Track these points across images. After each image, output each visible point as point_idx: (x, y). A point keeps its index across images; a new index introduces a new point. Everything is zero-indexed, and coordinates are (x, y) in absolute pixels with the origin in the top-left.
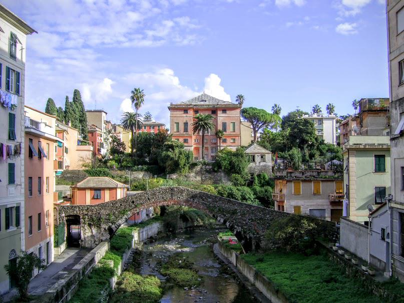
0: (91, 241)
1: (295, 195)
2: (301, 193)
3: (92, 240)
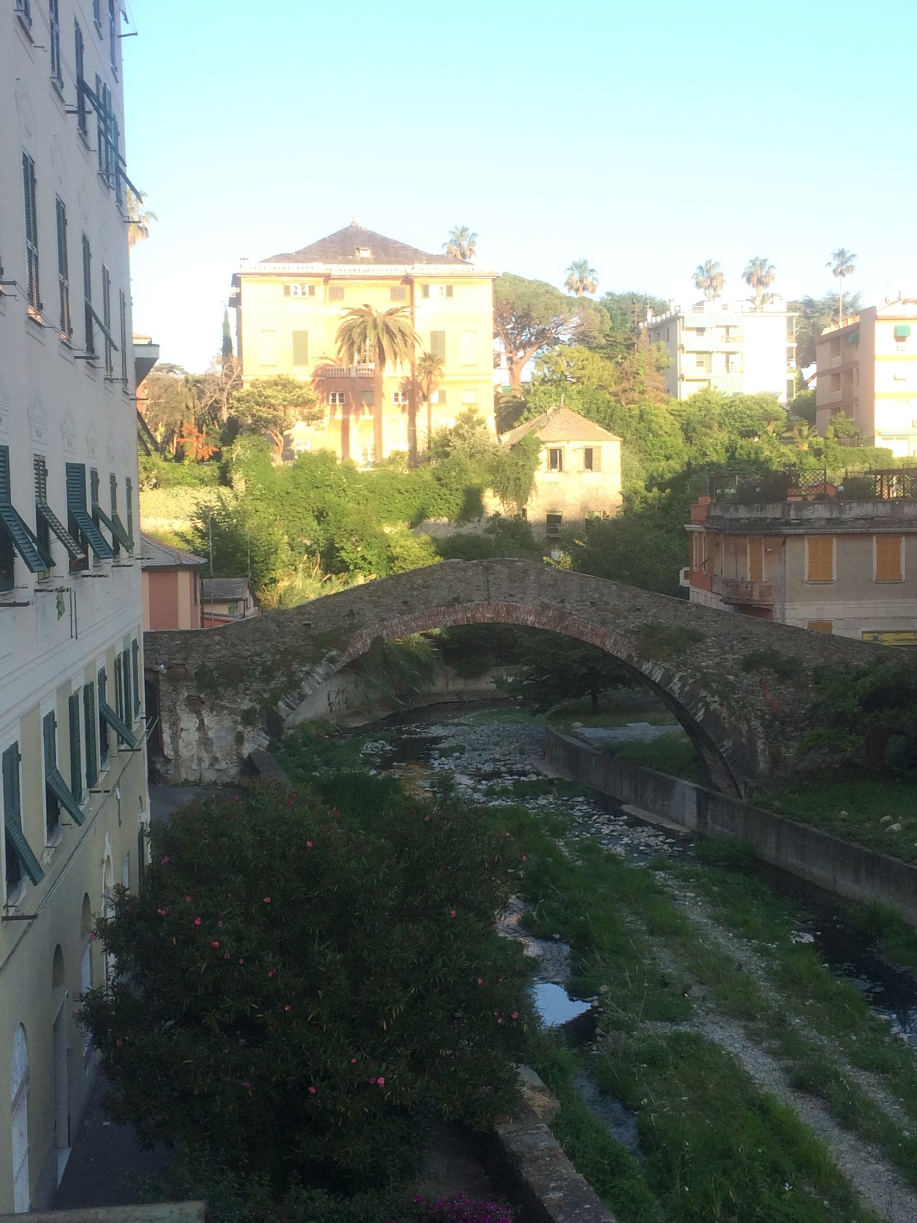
0: (200, 760)
1: (811, 582)
2: (834, 578)
3: (205, 755)
